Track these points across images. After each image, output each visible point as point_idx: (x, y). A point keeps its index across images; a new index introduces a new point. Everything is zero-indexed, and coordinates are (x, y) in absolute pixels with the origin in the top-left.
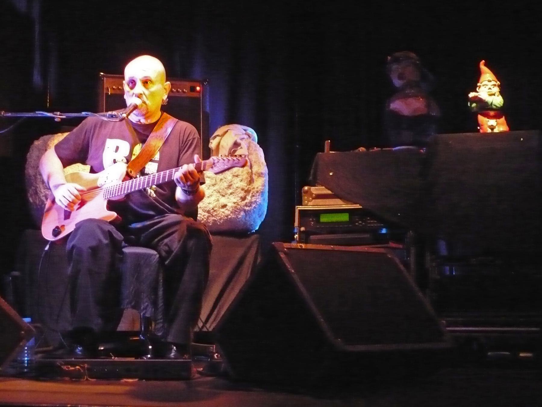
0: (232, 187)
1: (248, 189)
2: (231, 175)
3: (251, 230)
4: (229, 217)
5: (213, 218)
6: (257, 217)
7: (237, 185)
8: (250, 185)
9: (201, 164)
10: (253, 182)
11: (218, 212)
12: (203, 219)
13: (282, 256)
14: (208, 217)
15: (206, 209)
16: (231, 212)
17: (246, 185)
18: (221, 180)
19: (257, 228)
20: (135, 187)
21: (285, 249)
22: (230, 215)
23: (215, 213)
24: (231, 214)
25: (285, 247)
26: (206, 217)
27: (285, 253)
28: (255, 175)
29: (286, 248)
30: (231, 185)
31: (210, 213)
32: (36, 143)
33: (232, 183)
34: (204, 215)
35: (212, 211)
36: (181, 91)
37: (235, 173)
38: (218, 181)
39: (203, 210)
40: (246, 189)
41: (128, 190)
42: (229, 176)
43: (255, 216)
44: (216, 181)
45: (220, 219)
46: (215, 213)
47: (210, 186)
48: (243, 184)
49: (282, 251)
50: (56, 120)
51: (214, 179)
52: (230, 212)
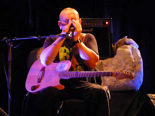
0: (125, 69)
1: (133, 70)
2: (125, 64)
3: (136, 90)
4: (125, 84)
5: (117, 85)
6: (138, 83)
7: (128, 68)
8: (134, 68)
9: (95, 74)
10: (136, 66)
11: (119, 82)
12: (112, 85)
13: (152, 100)
14: (114, 84)
15: (113, 80)
16: (126, 81)
17: (132, 68)
18: (120, 66)
19: (138, 89)
20: (73, 76)
21: (154, 97)
22: (125, 83)
23: (118, 82)
24: (126, 82)
25: (153, 96)
26: (113, 84)
27: (154, 99)
28: (136, 63)
29: (154, 97)
30: (125, 68)
31: (115, 82)
32: (32, 52)
33: (126, 67)
34: (112, 83)
35: (116, 81)
36: (96, 24)
37: (127, 62)
38: (118, 66)
39: (112, 81)
40: (132, 70)
41: (73, 76)
42: (124, 64)
43: (137, 83)
44: (117, 66)
45: (120, 85)
46: (118, 82)
47: (115, 69)
48: (131, 67)
49: (152, 98)
50: (38, 40)
51: (117, 66)
52: (125, 81)
